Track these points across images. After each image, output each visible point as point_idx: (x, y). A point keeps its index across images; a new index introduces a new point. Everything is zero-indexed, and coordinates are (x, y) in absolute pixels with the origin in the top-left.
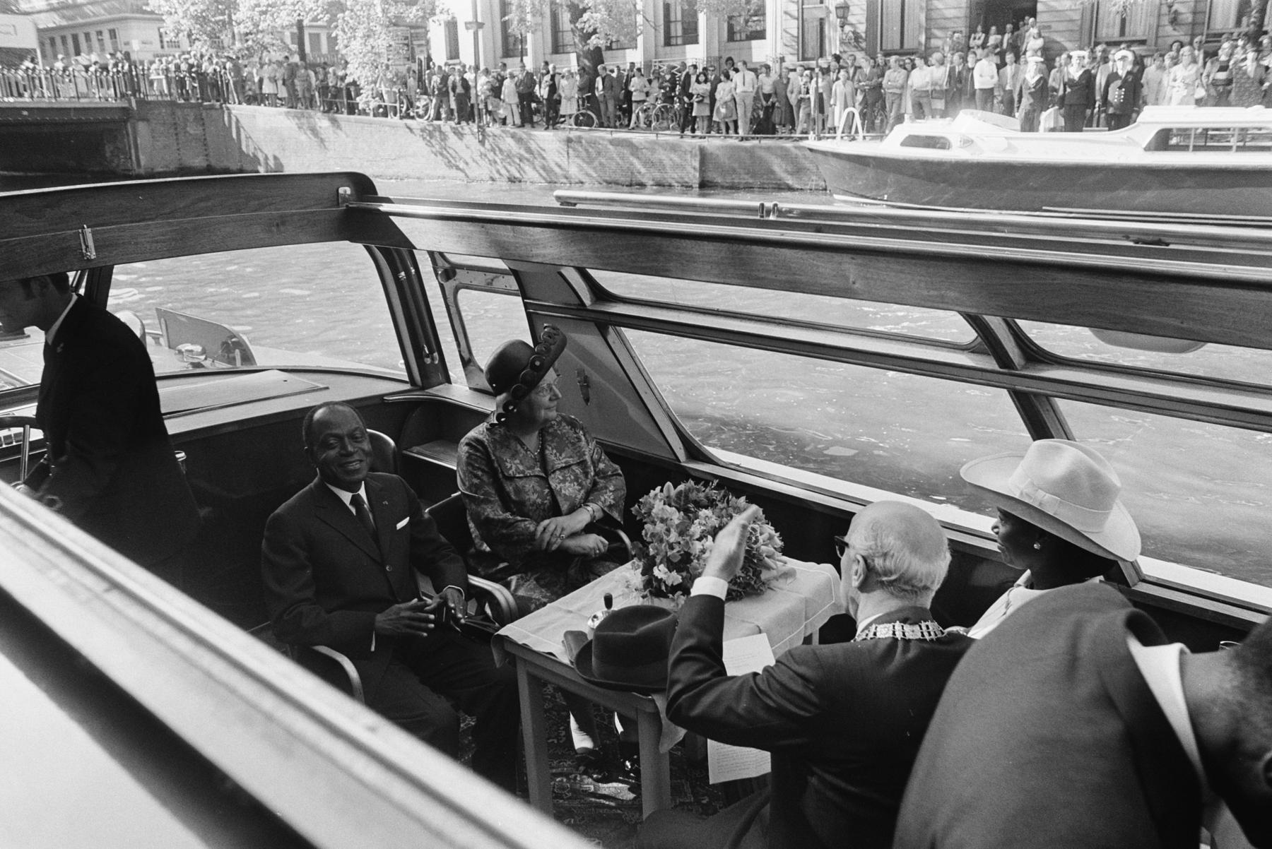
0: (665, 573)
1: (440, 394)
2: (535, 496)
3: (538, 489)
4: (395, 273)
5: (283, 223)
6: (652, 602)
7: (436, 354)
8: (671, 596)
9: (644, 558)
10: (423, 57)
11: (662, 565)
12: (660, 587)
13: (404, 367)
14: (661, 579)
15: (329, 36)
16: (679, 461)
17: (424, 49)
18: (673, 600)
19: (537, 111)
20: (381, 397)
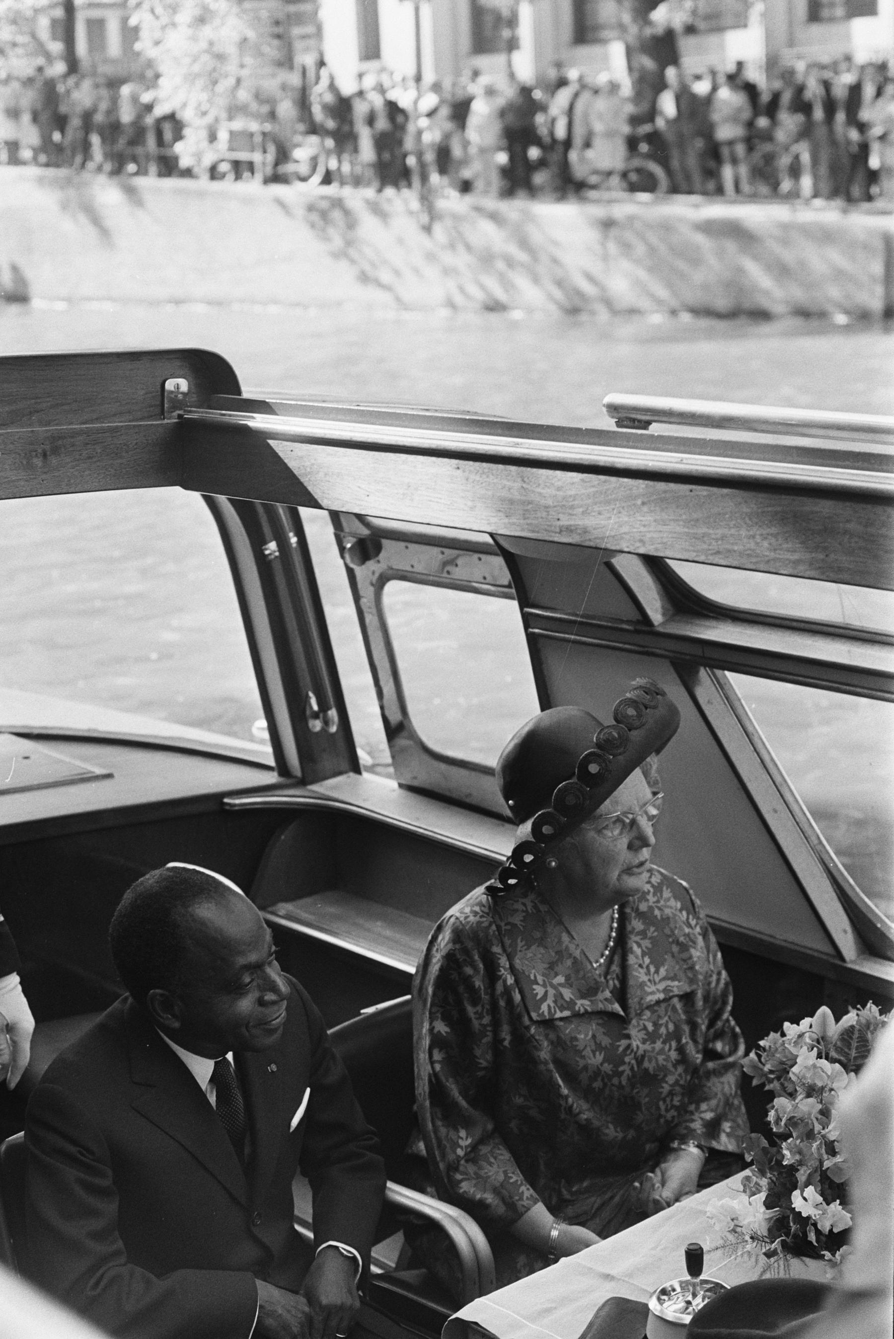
0: (817, 1206)
1: (335, 795)
2: (600, 1057)
3: (606, 1041)
4: (257, 543)
5: (55, 451)
6: (787, 1267)
7: (333, 713)
8: (827, 1255)
9: (771, 1169)
10: (308, 60)
11: (811, 1188)
12: (805, 1235)
13: (266, 735)
14: (809, 1218)
15: (125, 20)
16: (843, 959)
17: (312, 42)
18: (833, 1264)
19: (542, 163)
20: (217, 798)
